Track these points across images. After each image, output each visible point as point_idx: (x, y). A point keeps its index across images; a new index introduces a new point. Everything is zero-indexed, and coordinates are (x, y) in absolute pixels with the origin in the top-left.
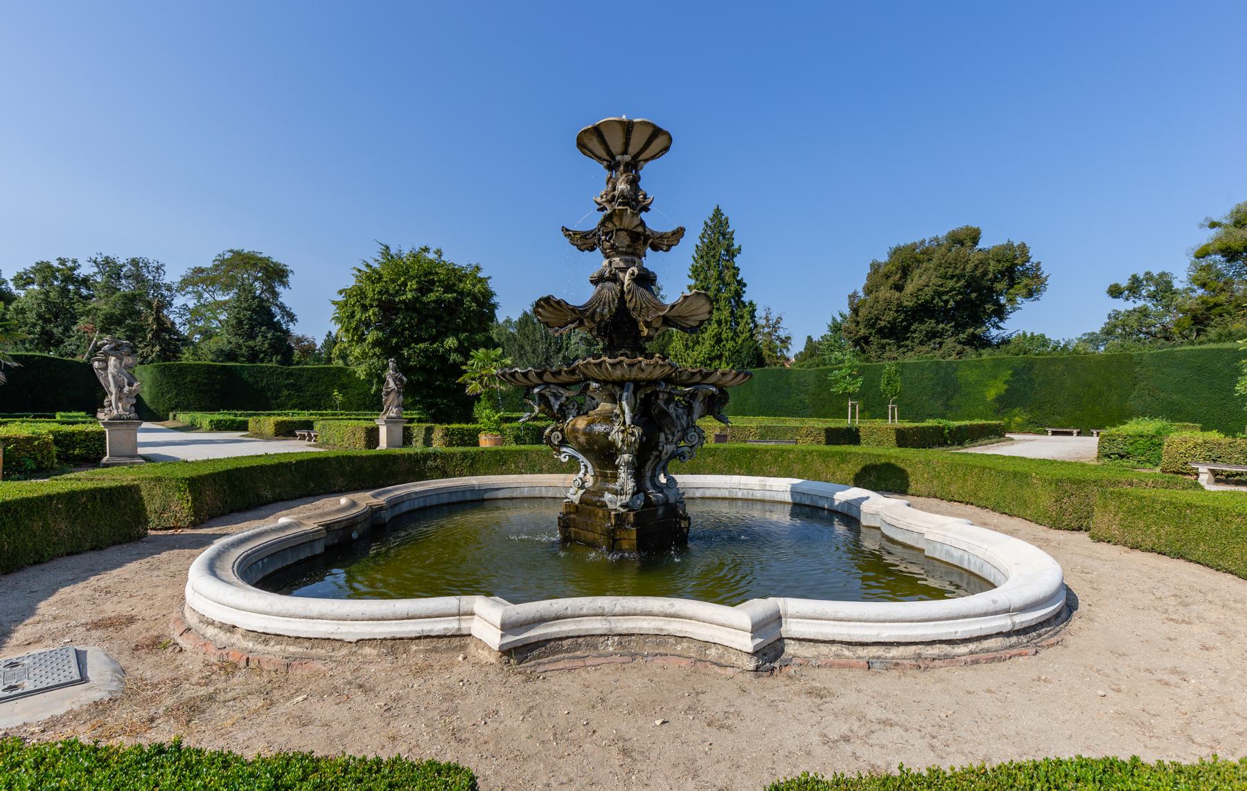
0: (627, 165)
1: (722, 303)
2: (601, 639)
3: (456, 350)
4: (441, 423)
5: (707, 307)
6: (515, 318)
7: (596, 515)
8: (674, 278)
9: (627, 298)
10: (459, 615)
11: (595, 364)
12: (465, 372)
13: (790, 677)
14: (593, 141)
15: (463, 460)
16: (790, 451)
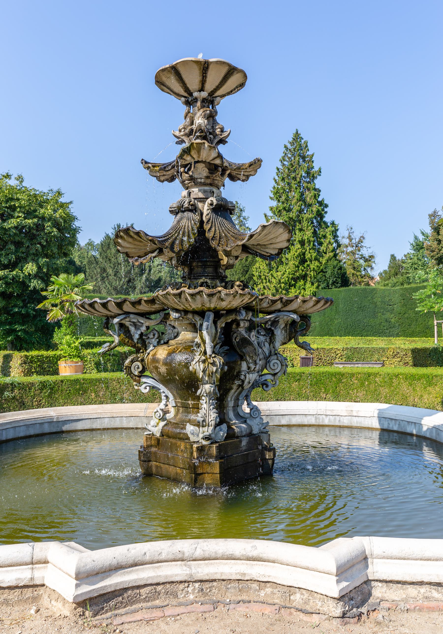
0: (204, 100)
1: (305, 224)
2: (181, 586)
3: (36, 276)
4: (19, 350)
5: (286, 236)
6: (98, 240)
7: (178, 447)
8: (255, 205)
9: (206, 227)
10: (32, 563)
11: (174, 295)
12: (45, 298)
13: (378, 623)
14: (171, 78)
15: (42, 389)
16: (376, 375)
